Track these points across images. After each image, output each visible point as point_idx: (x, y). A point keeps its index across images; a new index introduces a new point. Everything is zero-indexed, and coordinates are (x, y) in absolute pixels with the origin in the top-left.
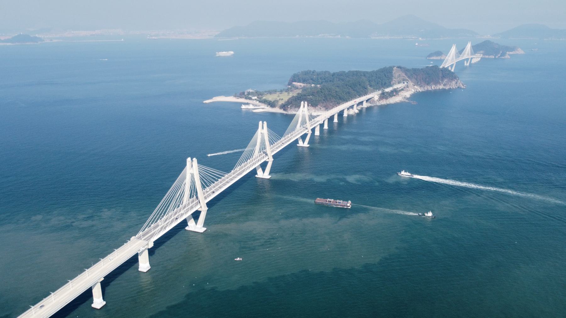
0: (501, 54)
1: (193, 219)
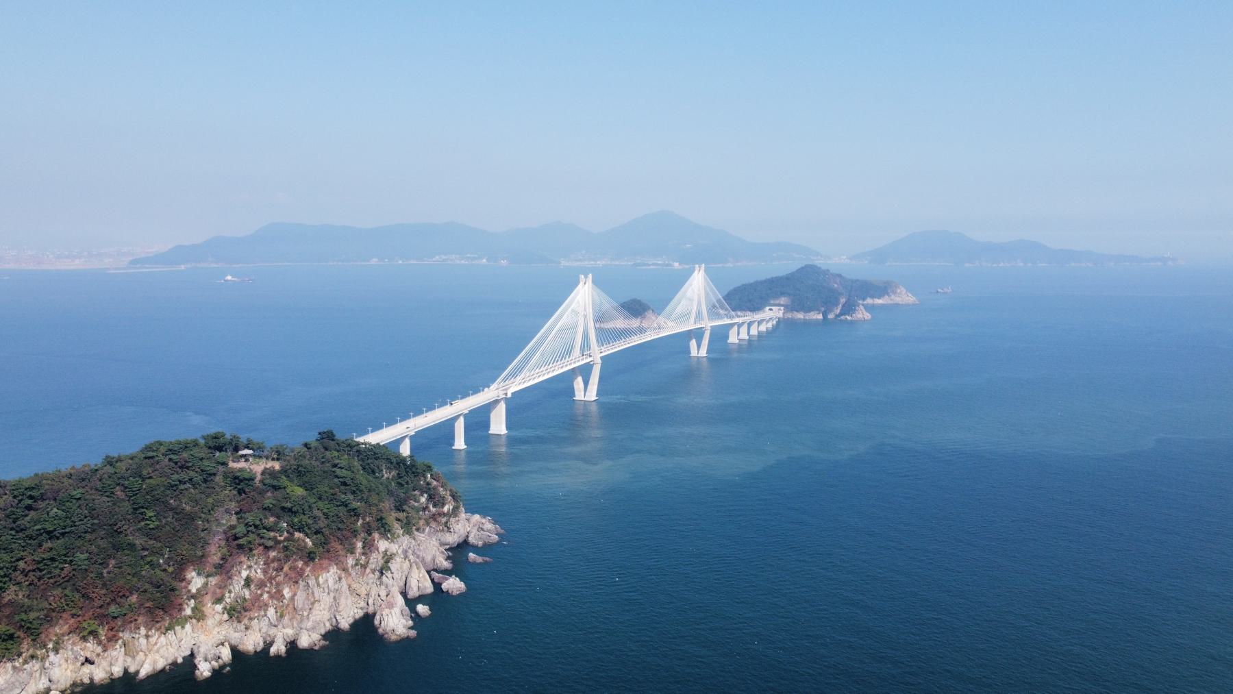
0: (843, 306)
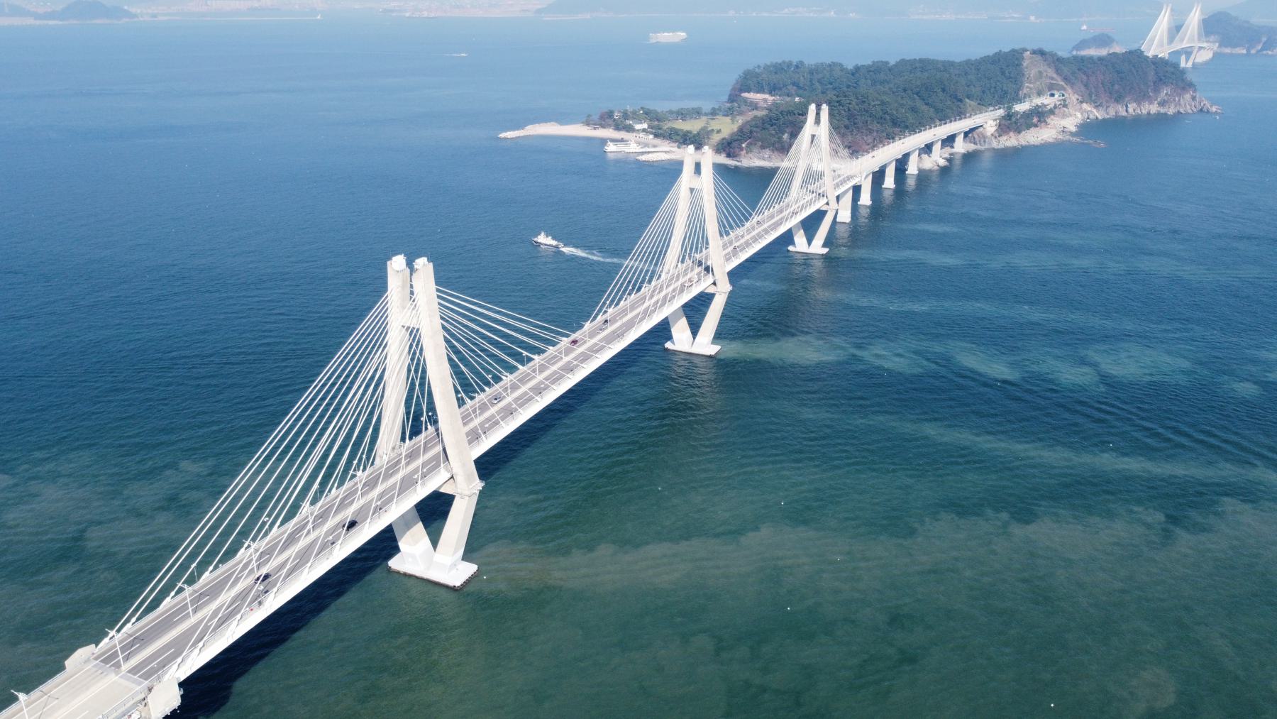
0: (1264, 43)
1: (420, 524)
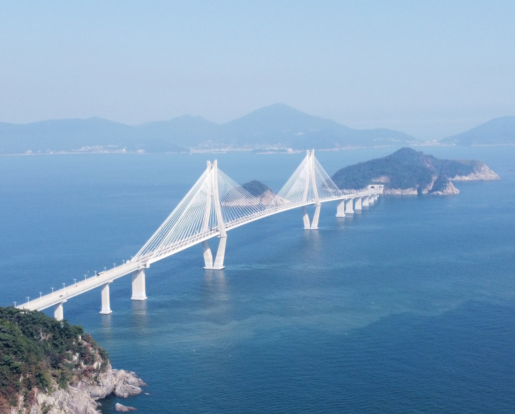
0: (435, 183)
